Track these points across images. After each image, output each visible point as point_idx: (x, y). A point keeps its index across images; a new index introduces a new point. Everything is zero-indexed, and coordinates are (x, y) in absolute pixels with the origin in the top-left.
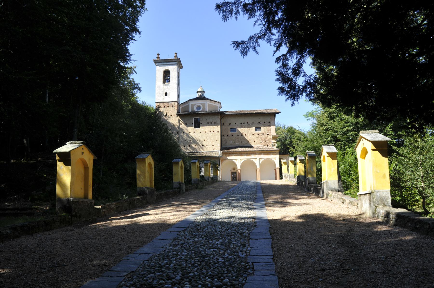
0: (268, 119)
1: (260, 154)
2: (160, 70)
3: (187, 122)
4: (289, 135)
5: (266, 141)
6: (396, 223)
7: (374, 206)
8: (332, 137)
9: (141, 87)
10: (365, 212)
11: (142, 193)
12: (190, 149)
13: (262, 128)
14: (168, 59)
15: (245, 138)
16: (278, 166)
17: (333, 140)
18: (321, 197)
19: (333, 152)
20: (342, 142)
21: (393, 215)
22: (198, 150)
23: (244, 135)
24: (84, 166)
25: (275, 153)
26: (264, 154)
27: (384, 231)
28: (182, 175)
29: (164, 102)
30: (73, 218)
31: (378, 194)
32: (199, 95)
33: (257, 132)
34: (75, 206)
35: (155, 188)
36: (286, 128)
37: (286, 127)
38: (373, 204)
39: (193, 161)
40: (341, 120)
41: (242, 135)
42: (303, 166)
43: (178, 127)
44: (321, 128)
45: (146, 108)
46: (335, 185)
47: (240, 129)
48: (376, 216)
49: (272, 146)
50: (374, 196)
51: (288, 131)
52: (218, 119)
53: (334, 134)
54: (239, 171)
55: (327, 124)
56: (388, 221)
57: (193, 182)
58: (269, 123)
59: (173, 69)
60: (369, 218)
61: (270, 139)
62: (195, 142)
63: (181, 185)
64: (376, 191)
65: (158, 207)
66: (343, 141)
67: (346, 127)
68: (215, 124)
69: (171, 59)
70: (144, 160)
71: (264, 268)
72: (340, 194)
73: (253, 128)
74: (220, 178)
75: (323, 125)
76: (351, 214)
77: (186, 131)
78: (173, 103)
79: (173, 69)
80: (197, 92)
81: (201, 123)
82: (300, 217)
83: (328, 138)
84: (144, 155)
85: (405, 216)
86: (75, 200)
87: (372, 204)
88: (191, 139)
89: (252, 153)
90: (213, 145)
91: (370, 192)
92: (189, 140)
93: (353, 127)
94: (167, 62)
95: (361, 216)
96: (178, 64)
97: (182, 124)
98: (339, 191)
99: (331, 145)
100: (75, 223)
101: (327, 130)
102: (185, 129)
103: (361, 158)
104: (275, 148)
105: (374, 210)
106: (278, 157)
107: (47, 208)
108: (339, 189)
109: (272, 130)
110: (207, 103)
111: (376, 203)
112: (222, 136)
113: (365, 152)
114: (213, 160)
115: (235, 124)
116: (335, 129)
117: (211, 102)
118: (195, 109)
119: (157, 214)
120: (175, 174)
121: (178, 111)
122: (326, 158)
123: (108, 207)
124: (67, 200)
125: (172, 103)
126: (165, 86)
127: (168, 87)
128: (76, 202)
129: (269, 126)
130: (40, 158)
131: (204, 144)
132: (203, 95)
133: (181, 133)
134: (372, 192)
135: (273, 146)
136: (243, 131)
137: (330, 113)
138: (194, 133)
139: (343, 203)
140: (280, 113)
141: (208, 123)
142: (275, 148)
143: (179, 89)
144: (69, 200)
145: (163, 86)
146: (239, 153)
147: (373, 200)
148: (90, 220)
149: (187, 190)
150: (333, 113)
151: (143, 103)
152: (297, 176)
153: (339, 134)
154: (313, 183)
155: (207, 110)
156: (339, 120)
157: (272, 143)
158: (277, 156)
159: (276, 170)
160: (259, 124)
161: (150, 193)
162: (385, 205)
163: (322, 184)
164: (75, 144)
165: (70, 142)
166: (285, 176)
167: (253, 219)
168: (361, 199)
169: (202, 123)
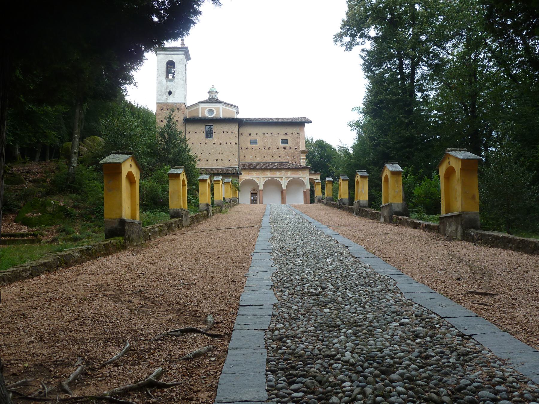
28: (209, 196)
31: (467, 216)
37: (314, 141)
39: (215, 179)
63: (209, 207)
71: (401, 279)
81: (215, 133)
90: (229, 160)
110: (221, 107)
120: (202, 194)
126: (168, 83)
127: (173, 83)
145: (166, 82)
155: (221, 116)
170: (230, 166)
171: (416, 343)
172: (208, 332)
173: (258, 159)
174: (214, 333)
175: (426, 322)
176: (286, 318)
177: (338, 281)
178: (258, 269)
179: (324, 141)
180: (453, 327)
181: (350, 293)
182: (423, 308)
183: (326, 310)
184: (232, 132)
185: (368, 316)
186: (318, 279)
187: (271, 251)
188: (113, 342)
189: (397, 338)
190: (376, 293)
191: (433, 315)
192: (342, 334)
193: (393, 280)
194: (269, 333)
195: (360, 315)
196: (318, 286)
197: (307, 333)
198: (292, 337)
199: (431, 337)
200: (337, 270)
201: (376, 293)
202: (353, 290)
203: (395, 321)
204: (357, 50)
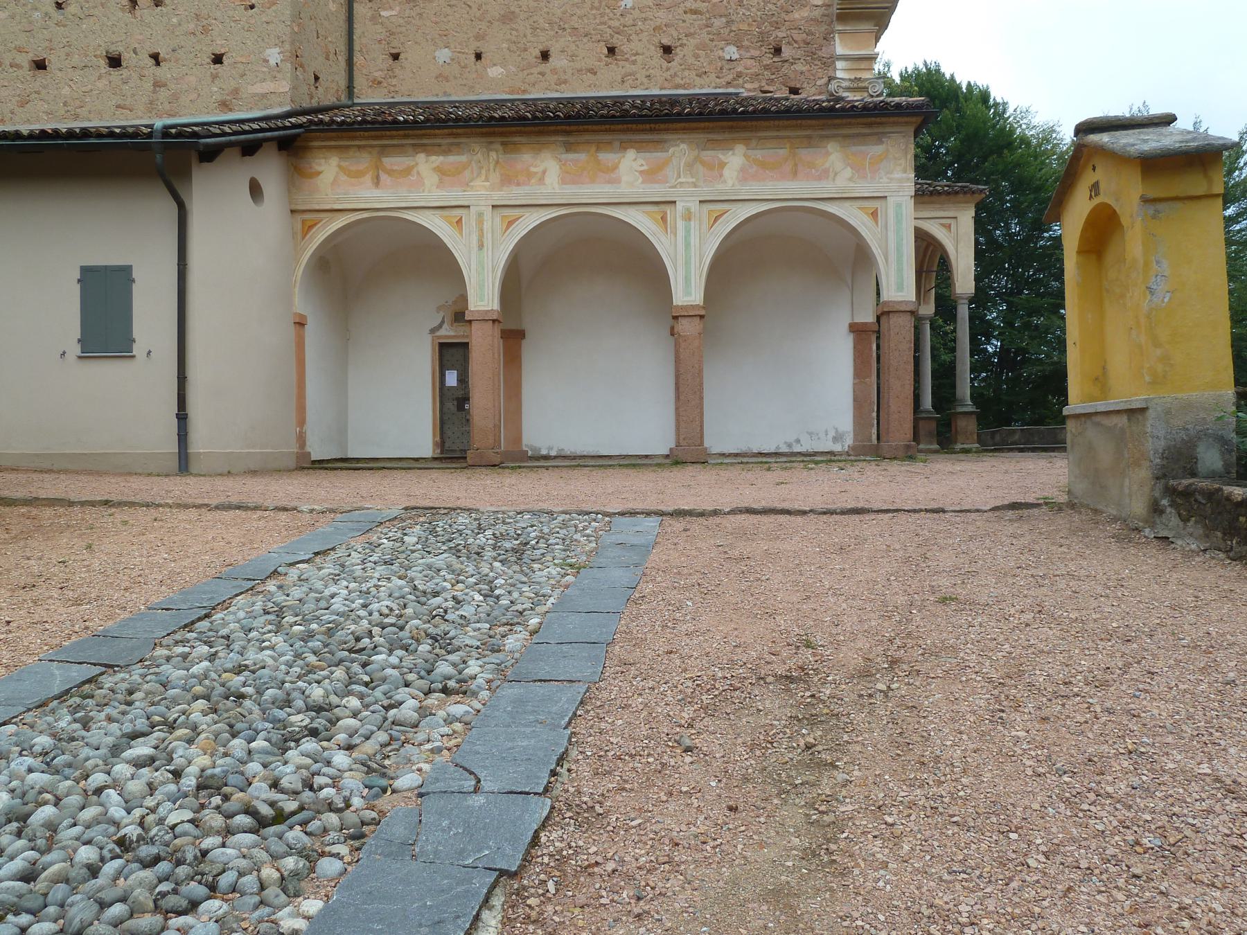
90: (218, 59)
170: (225, 105)
173: (495, 72)
179: (947, 71)
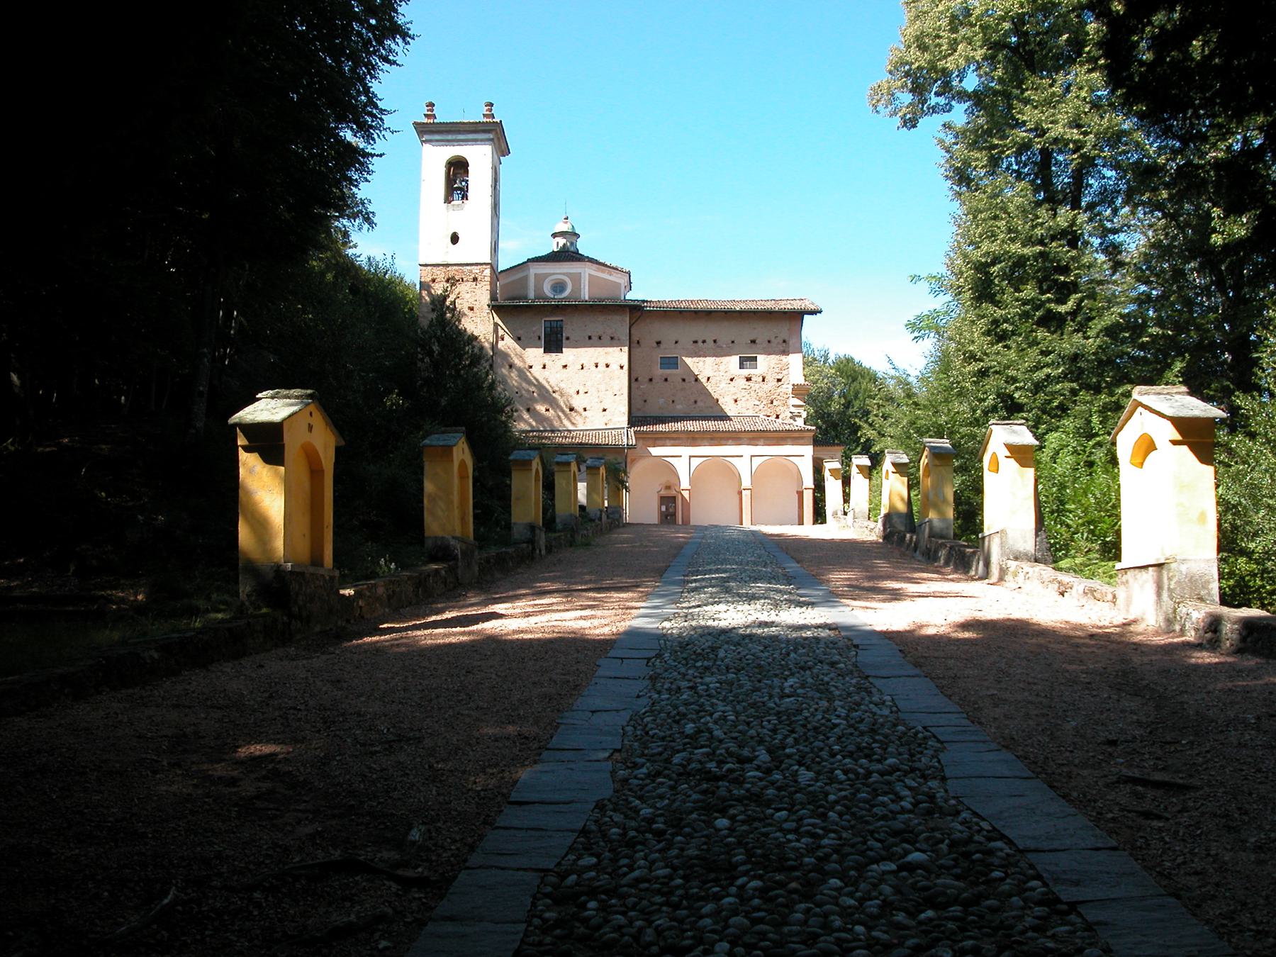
0: (782, 330)
1: (752, 442)
2: (436, 157)
3: (521, 332)
4: (840, 384)
5: (772, 403)
6: (1241, 645)
7: (1172, 600)
8: (998, 395)
9: (373, 213)
10: (1139, 618)
11: (442, 552)
12: (531, 420)
13: (760, 358)
14: (464, 123)
15: (705, 388)
16: (809, 482)
17: (1002, 407)
18: (981, 579)
19: (1025, 443)
20: (1029, 412)
21: (1235, 623)
22: (556, 424)
23: (703, 380)
24: (310, 467)
25: (802, 441)
26: (767, 442)
27: (1216, 663)
28: (537, 503)
29: (447, 265)
30: (293, 622)
31: (1184, 568)
32: (561, 245)
33: (746, 372)
34: (297, 587)
35: (475, 539)
36: (830, 361)
37: (832, 358)
38: (1169, 596)
40: (1031, 345)
41: (697, 380)
42: (903, 483)
43: (494, 347)
44: (964, 367)
45: (381, 281)
46: (1025, 542)
47: (690, 359)
48: (1177, 628)
49: (791, 418)
50: (1171, 574)
51: (838, 370)
52: (621, 325)
53: (1006, 388)
54: (686, 494)
55: (986, 354)
56: (1216, 642)
57: (560, 527)
58: (784, 344)
59: (479, 156)
60: (1157, 633)
61: (786, 396)
62: (546, 395)
63: (537, 531)
64: (1178, 558)
65: (500, 598)
66: (1032, 409)
67: (1044, 367)
68: (613, 341)
69: (473, 123)
70: (447, 450)
72: (1047, 571)
73: (733, 357)
74: (628, 515)
75: (972, 357)
76: (1101, 624)
77: (517, 362)
78: (476, 270)
79: (479, 156)
80: (554, 235)
81: (568, 338)
82: (965, 626)
83: (987, 398)
84: (445, 436)
85: (1270, 625)
86: (296, 570)
87: (1165, 595)
88: (532, 389)
89: (728, 439)
90: (605, 410)
91: (1162, 561)
92: (528, 391)
93: (1067, 369)
94: (459, 132)
95: (1132, 628)
96: (496, 140)
97: (506, 337)
98: (1036, 561)
99: (1016, 422)
100: (298, 637)
101: (983, 373)
102: (516, 355)
103: (1132, 464)
104: (800, 423)
105: (1171, 611)
106: (811, 453)
107: (140, 597)
108: (1039, 555)
109: (794, 369)
110: (586, 271)
111: (1178, 591)
112: (633, 380)
113: (1147, 446)
114: (610, 457)
115: (676, 342)
116: (1011, 373)
117: (598, 270)
118: (547, 290)
119: (527, 615)
120: (518, 499)
121: (493, 297)
122: (1002, 461)
123: (368, 594)
124: (275, 568)
125: (476, 267)
128: (297, 574)
129: (785, 352)
130: (67, 437)
131: (577, 403)
132: (572, 244)
133: (503, 366)
134: (1167, 561)
135: (793, 418)
136: (702, 366)
137: (996, 322)
138: (544, 367)
139: (1062, 594)
140: (820, 312)
141: (590, 338)
142: (800, 423)
143: (496, 222)
144: (281, 568)
146: (688, 438)
147: (1169, 585)
148: (331, 629)
149: (549, 549)
150: (1006, 321)
151: (370, 265)
152: (882, 515)
153: (1021, 388)
154: (942, 537)
155: (585, 294)
156: (1024, 346)
157: (793, 409)
158: (808, 451)
159: (800, 494)
160: (753, 345)
161: (464, 553)
162: (1201, 599)
163: (983, 538)
164: (289, 398)
165: (270, 392)
166: (835, 514)
167: (830, 629)
168: (1127, 581)
169: (572, 338)
171: (920, 923)
172: (400, 872)
174: (410, 873)
175: (973, 862)
176: (611, 841)
177: (790, 740)
178: (598, 703)
179: (857, 360)
180: (1038, 877)
181: (805, 776)
182: (982, 824)
183: (722, 823)
184: (612, 338)
185: (825, 841)
186: (737, 734)
187: (653, 654)
188: (138, 889)
189: (873, 906)
190: (875, 777)
191: (999, 844)
192: (733, 890)
193: (938, 741)
194: (553, 879)
195: (803, 840)
196: (731, 754)
197: (646, 885)
198: (606, 892)
199: (966, 904)
200: (799, 711)
201: (875, 777)
202: (817, 768)
203: (890, 858)
204: (931, 125)
